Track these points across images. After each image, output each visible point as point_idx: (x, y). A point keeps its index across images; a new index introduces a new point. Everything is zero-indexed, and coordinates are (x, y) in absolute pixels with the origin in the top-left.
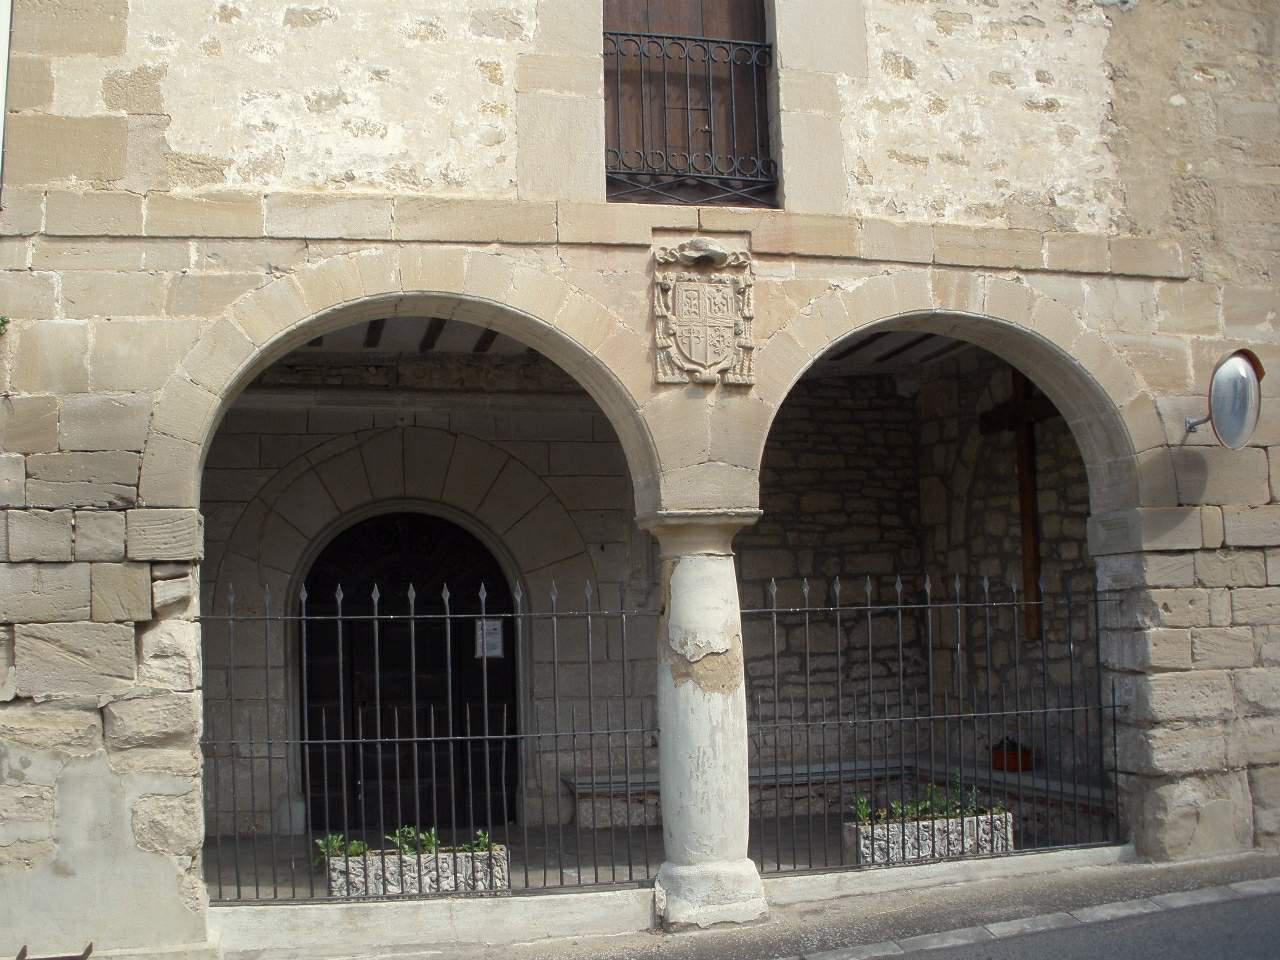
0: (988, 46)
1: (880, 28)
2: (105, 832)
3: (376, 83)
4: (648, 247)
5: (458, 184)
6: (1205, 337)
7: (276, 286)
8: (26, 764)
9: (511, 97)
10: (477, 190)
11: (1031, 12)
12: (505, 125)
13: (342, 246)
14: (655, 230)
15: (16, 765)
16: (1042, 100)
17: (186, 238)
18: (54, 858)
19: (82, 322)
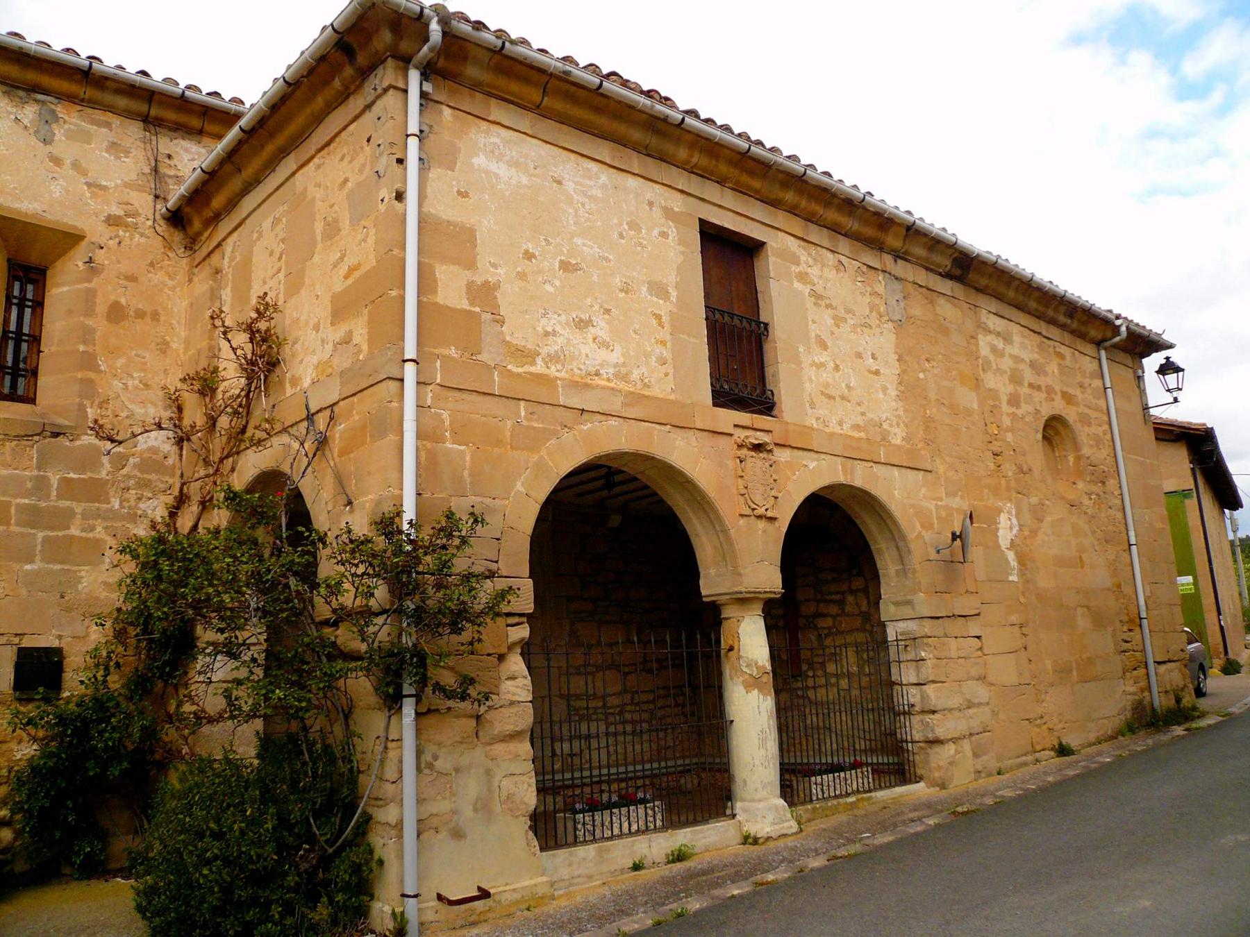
0: (853, 336)
1: (814, 322)
2: (483, 807)
3: (607, 317)
4: (731, 435)
5: (649, 387)
6: (939, 503)
7: (567, 436)
8: (436, 758)
9: (668, 337)
10: (656, 392)
11: (867, 321)
12: (667, 354)
13: (599, 417)
14: (735, 426)
15: (429, 758)
16: (874, 369)
17: (519, 399)
18: (454, 824)
19: (462, 448)
